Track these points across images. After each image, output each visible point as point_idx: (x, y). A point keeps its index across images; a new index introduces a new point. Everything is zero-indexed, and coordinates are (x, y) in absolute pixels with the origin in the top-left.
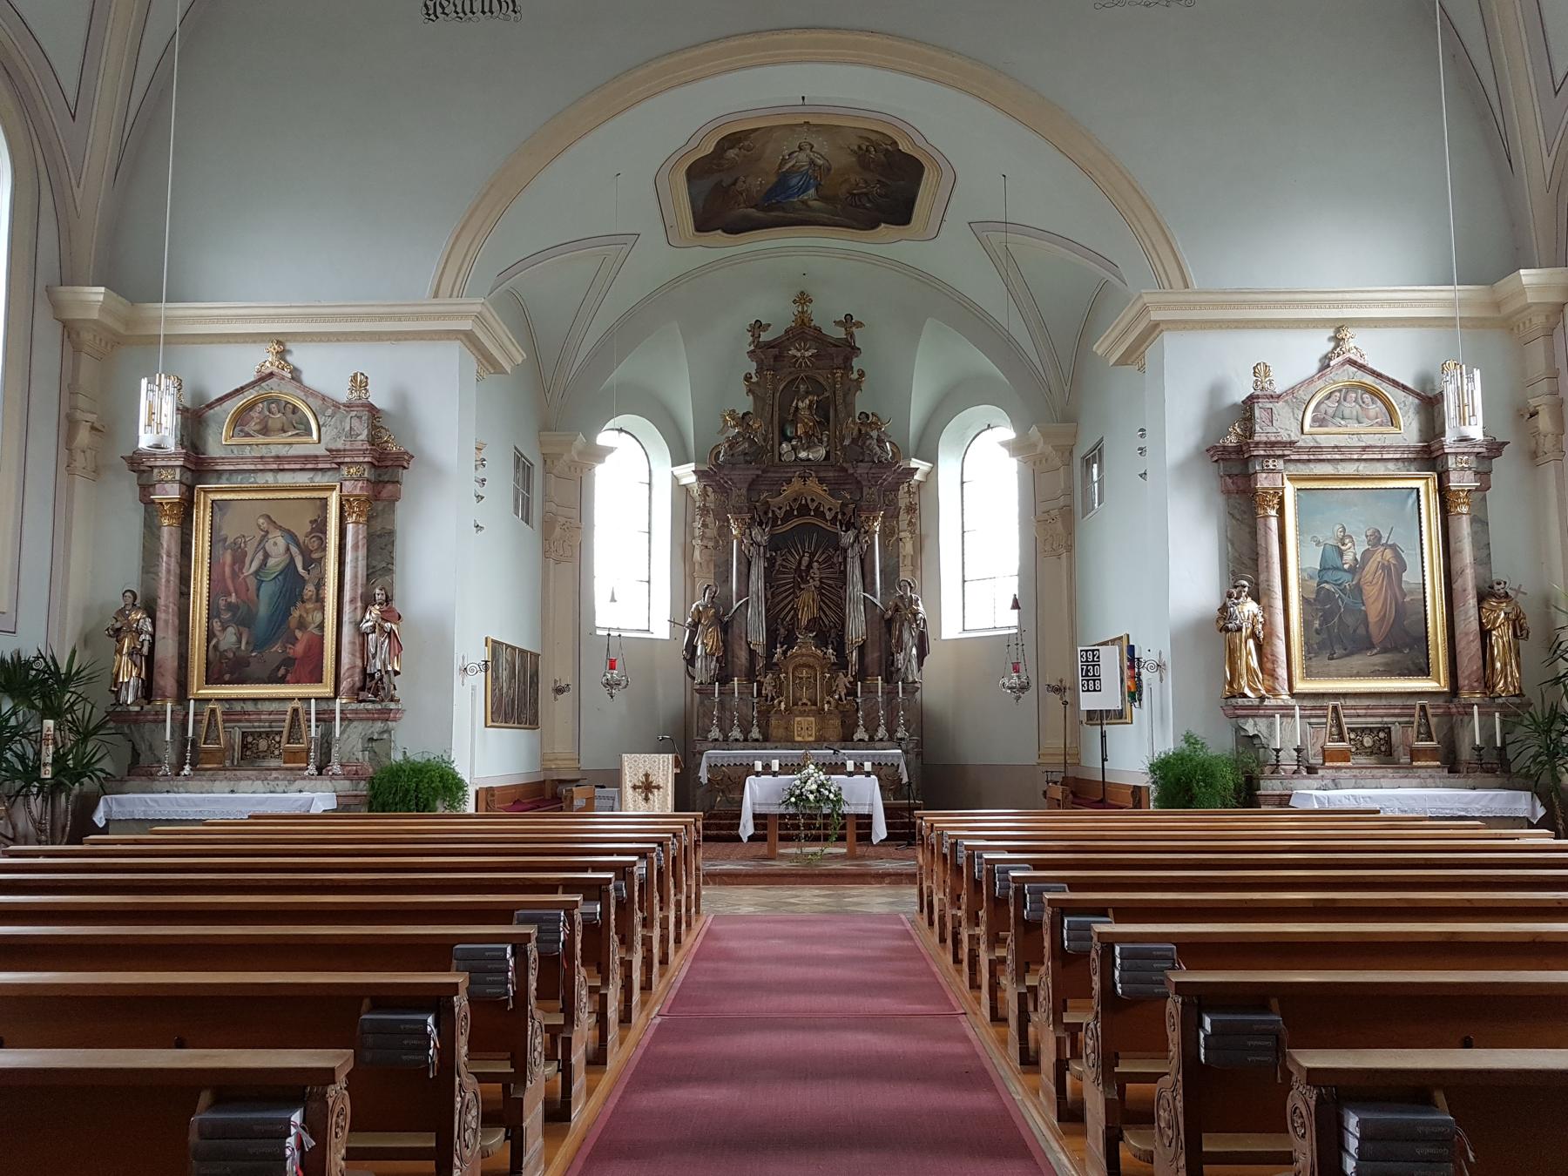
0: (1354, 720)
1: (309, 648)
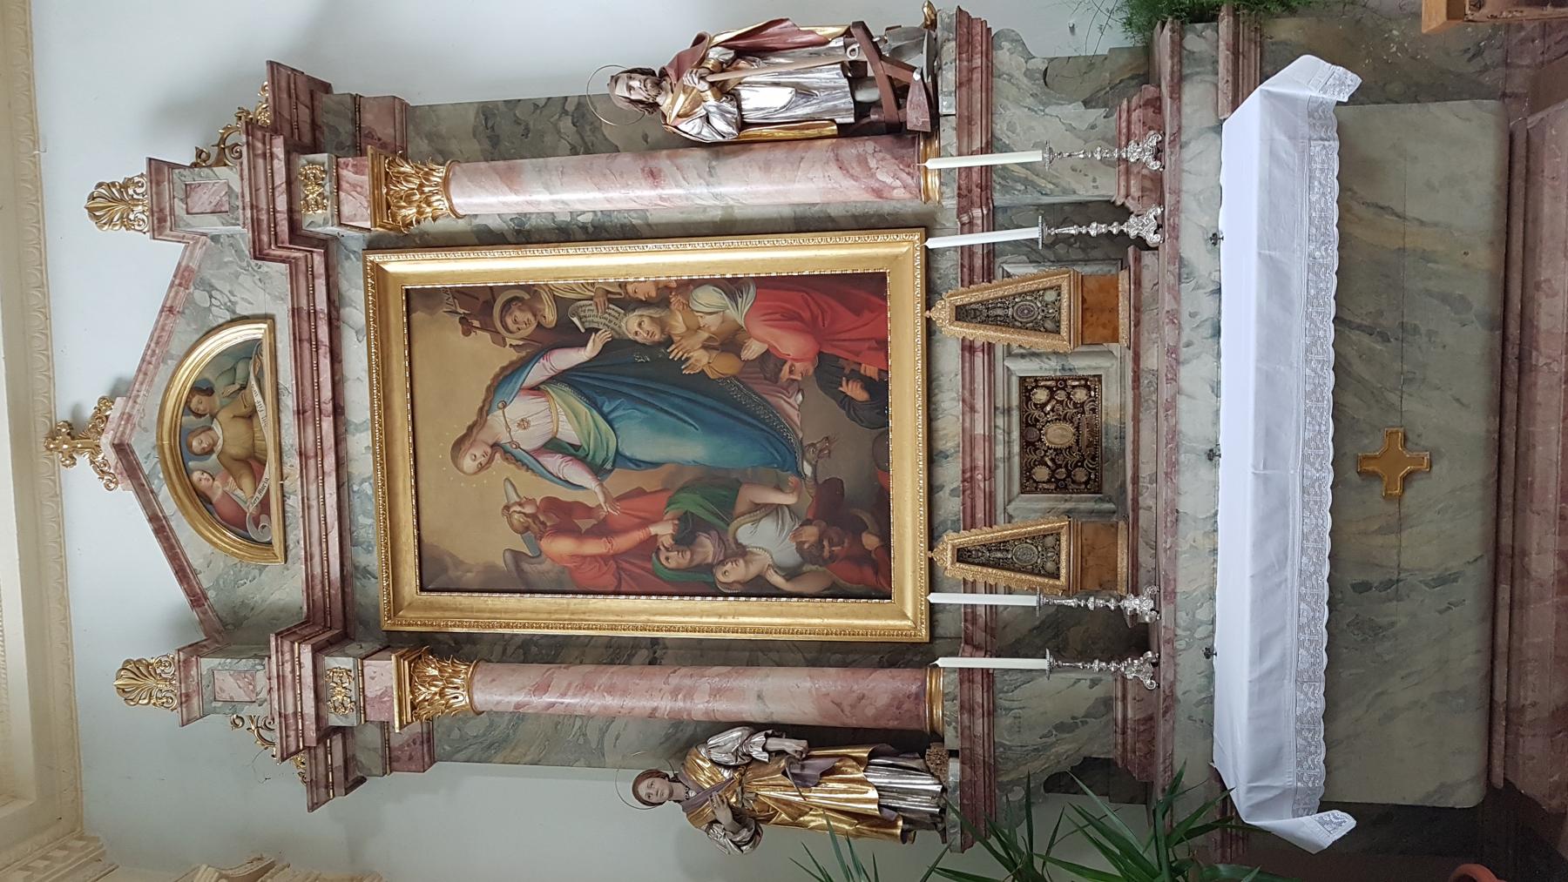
1: (788, 319)
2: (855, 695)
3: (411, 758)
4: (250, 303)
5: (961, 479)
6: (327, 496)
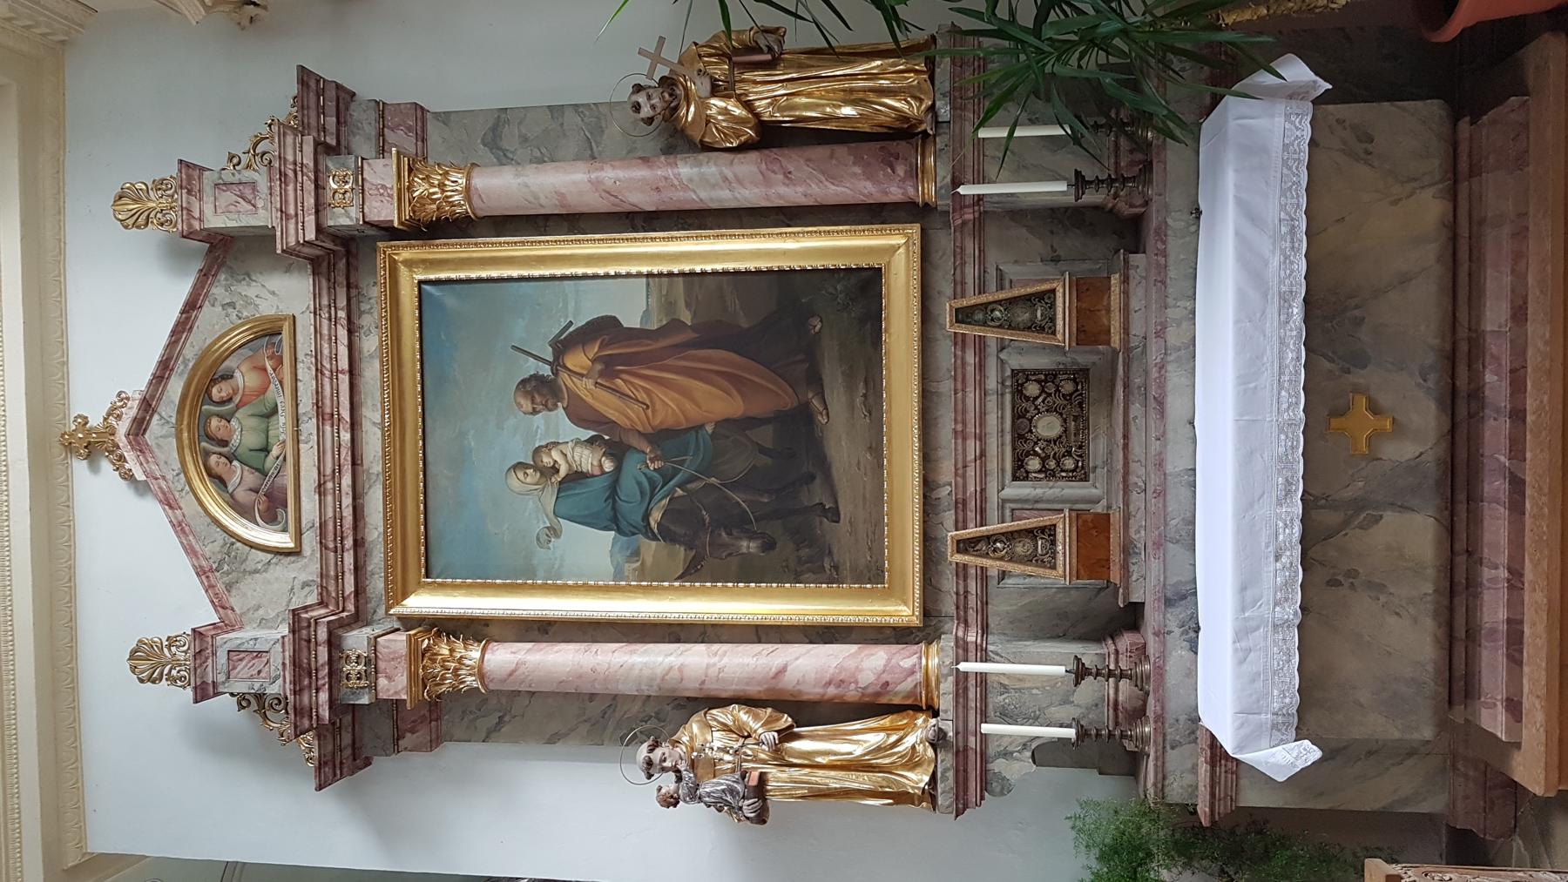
0: (993, 465)
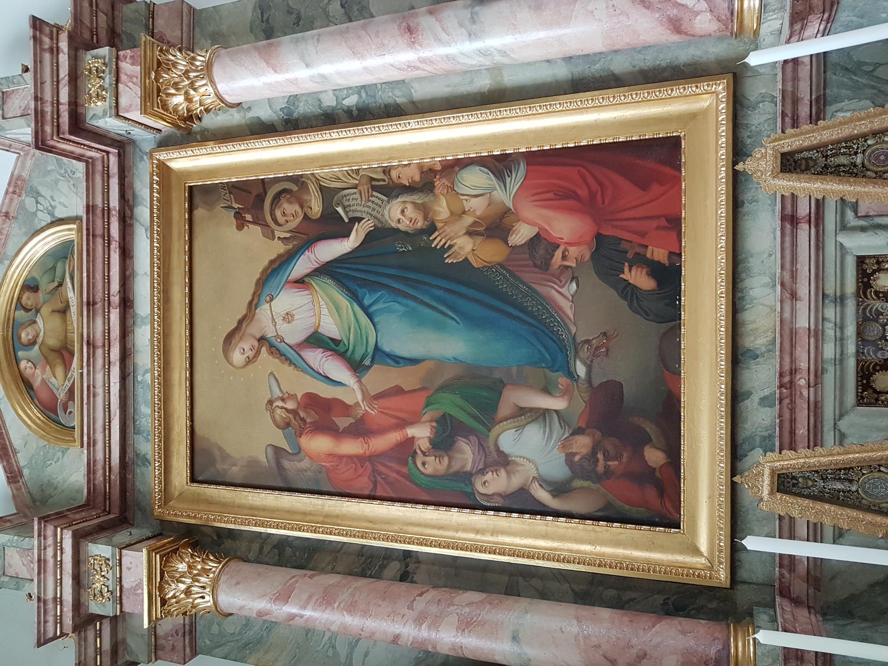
2: (634, 651)
3: (173, 648)
4: (66, 207)
5: (777, 383)
6: (112, 384)
